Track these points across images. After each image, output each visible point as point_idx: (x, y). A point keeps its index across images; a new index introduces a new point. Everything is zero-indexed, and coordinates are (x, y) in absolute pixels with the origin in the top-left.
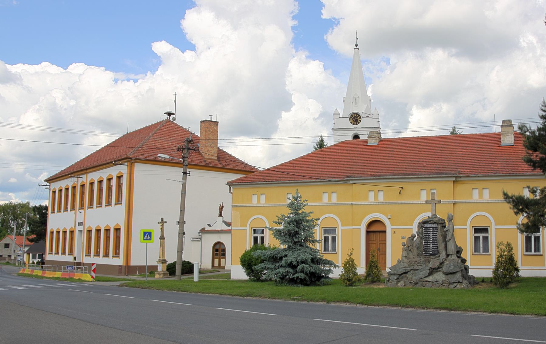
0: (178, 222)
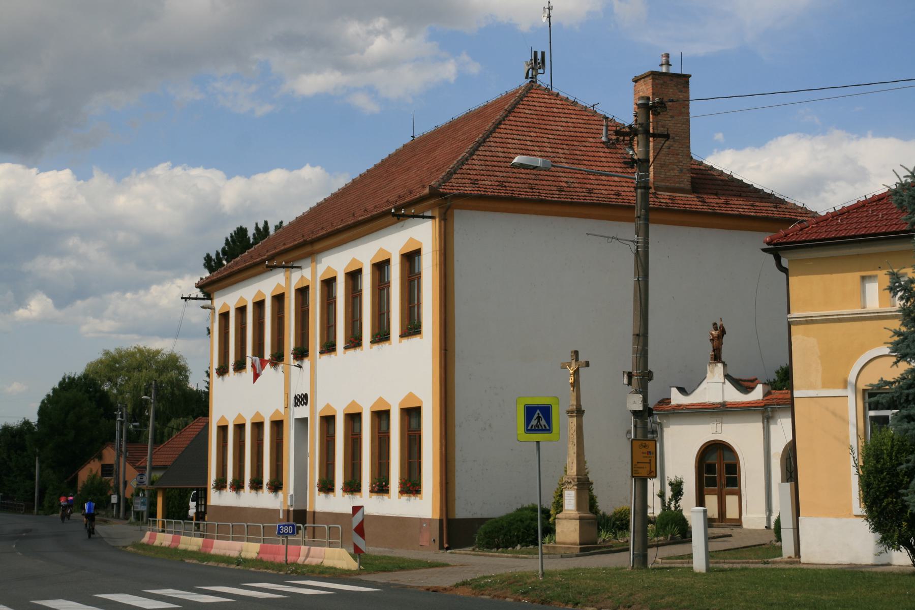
0: (630, 376)
